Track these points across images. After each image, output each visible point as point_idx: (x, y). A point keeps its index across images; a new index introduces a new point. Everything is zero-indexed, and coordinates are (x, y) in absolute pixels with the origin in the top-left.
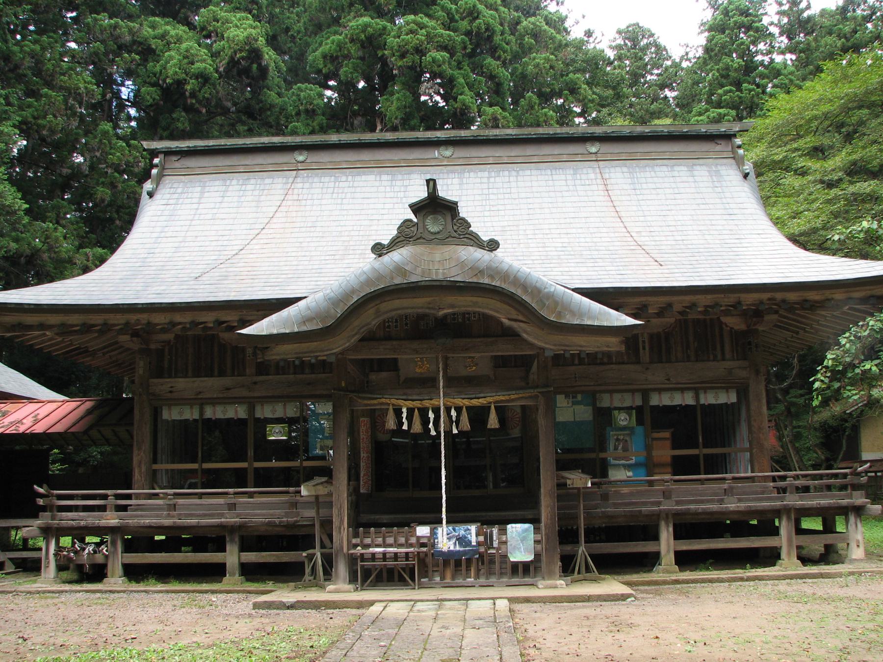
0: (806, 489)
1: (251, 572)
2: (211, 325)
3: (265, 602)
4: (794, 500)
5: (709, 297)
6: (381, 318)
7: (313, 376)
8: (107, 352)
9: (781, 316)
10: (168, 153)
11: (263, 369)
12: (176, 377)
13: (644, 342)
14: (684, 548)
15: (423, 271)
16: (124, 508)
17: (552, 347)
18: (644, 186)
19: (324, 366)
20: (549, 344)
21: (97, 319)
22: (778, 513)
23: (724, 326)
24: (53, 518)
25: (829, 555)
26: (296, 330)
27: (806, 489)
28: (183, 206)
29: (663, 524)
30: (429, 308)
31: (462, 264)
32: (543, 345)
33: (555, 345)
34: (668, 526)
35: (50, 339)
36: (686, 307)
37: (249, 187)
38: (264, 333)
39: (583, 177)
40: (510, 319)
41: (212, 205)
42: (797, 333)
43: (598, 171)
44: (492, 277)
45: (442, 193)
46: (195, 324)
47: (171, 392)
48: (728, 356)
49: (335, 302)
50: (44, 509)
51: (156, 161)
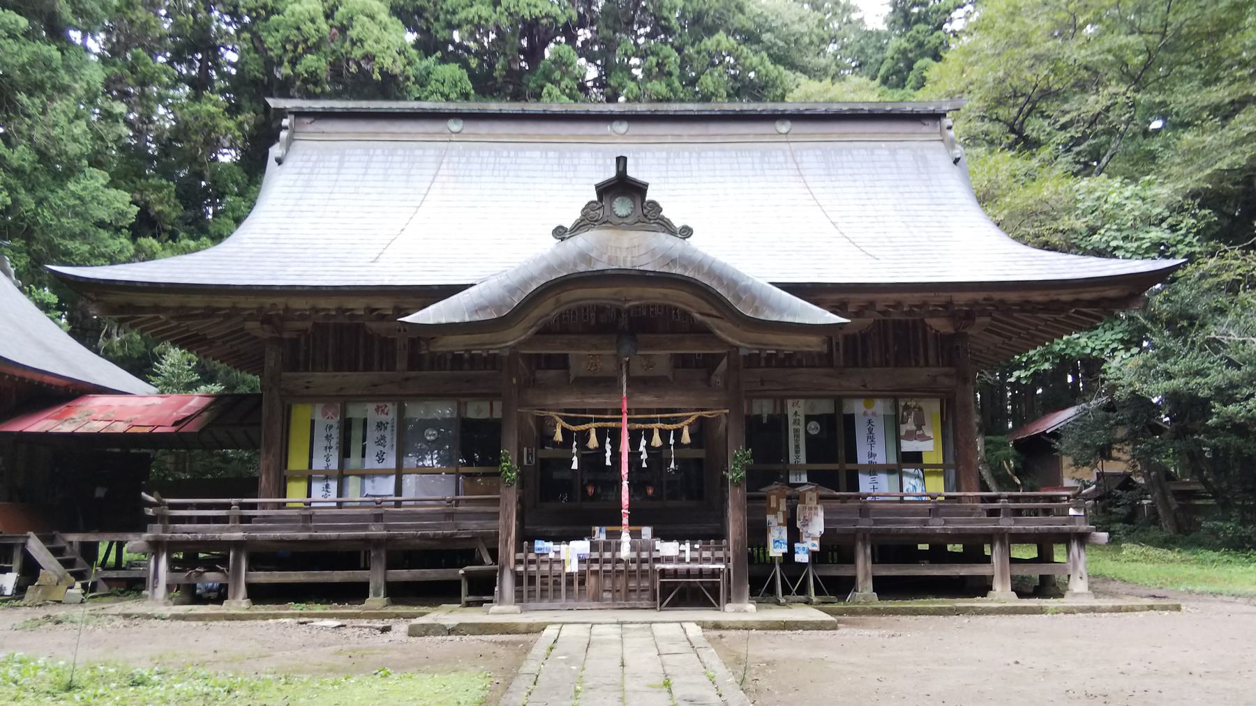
0: (1018, 512)
1: (399, 593)
2: (333, 313)
3: (423, 625)
4: (1006, 524)
5: (917, 295)
6: (562, 309)
7: (473, 372)
8: (227, 342)
9: (994, 319)
10: (299, 114)
11: (415, 362)
12: (314, 370)
13: (838, 344)
14: (884, 573)
15: (610, 259)
16: (248, 519)
17: (748, 346)
18: (840, 171)
19: (492, 361)
20: (745, 342)
21: (224, 302)
22: (990, 537)
23: (928, 329)
24: (165, 531)
25: (1046, 588)
26: (467, 319)
27: (1018, 512)
28: (320, 177)
29: (859, 546)
30: (615, 300)
31: (652, 252)
32: (738, 343)
33: (750, 343)
34: (865, 548)
35: (166, 323)
36: (890, 306)
37: (397, 159)
38: (431, 322)
39: (772, 160)
40: (702, 314)
41: (355, 177)
42: (1010, 338)
43: (788, 153)
44: (685, 267)
45: (631, 172)
46: (342, 310)
47: (307, 388)
48: (931, 361)
49: (512, 291)
50: (153, 520)
51: (285, 122)
